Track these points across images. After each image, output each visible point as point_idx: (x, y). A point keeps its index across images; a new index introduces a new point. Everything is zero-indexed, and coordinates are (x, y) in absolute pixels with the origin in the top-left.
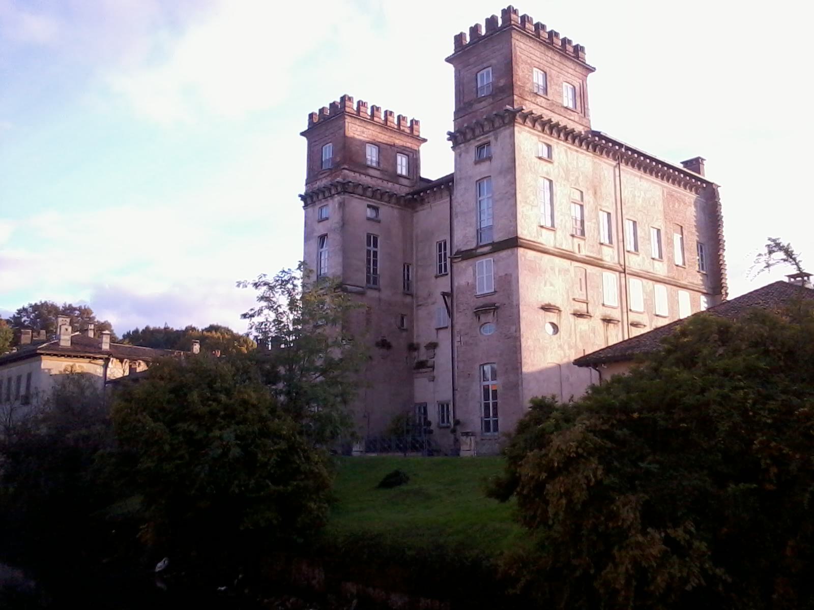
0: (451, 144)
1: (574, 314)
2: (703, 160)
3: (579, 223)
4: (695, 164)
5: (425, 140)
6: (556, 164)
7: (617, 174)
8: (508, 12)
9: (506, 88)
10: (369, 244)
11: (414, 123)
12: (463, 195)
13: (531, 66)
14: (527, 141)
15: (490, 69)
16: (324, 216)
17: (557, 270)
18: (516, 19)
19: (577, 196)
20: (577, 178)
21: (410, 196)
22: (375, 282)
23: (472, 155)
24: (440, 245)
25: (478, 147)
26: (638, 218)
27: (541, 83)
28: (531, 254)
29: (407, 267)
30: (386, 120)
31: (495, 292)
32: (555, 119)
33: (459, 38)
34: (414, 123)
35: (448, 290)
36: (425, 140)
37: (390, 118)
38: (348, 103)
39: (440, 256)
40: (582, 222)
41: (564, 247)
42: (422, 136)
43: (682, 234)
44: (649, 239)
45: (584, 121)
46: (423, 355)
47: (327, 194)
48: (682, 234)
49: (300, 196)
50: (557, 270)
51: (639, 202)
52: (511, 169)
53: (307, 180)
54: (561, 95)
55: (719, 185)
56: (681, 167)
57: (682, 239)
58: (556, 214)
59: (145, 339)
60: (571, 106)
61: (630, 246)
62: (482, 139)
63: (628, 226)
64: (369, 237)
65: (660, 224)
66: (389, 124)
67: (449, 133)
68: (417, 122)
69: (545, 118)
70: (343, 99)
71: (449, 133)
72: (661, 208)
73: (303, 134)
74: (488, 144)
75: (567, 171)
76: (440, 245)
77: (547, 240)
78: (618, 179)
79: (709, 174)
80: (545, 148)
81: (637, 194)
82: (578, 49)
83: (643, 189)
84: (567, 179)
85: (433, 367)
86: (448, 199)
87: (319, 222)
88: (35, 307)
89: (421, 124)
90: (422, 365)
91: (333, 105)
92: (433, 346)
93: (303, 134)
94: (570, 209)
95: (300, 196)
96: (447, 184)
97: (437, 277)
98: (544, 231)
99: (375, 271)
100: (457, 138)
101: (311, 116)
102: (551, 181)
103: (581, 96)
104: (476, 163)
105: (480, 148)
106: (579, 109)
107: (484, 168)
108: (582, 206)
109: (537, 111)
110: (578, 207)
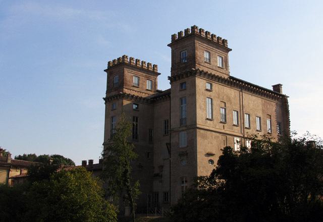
0: (169, 81)
1: (214, 155)
2: (281, 85)
3: (224, 116)
4: (277, 87)
5: (160, 74)
6: (214, 91)
7: (241, 94)
8: (194, 28)
9: (193, 59)
10: (134, 121)
11: (155, 66)
12: (175, 102)
13: (203, 54)
14: (201, 84)
15: (186, 51)
16: (114, 108)
17: (214, 137)
18: (197, 31)
19: (223, 105)
20: (223, 97)
21: (152, 99)
22: (136, 138)
23: (178, 88)
24: (166, 122)
25: (181, 84)
26: (251, 113)
27: (208, 57)
28: (202, 131)
29: (151, 131)
30: (142, 65)
31: (187, 146)
32: (213, 73)
33: (173, 36)
34: (155, 66)
35: (168, 142)
36: (160, 74)
37: (144, 65)
38: (126, 59)
39: (166, 131)
40: (225, 115)
41: (217, 127)
42: (158, 72)
43: (271, 119)
44: (256, 122)
45: (227, 72)
46: (157, 171)
47: (115, 98)
48: (271, 119)
49: (103, 98)
50: (214, 137)
51: (251, 106)
52: (194, 94)
53: (107, 91)
54: (217, 62)
55: (288, 96)
56: (272, 89)
57: (271, 121)
58: (214, 113)
59: (24, 161)
60: (221, 66)
61: (247, 125)
62: (182, 81)
63: (246, 117)
64: (134, 117)
65: (260, 114)
66: (144, 67)
67: (169, 77)
68: (156, 66)
69: (209, 73)
70: (123, 57)
71: (169, 77)
72: (261, 108)
73: (105, 71)
74: (185, 83)
75: (219, 95)
76: (166, 122)
77: (210, 125)
78: (241, 96)
79: (284, 92)
80: (209, 85)
81: (250, 102)
82: (224, 41)
83: (252, 102)
84: (219, 98)
85: (162, 176)
86: (169, 101)
87: (112, 110)
88: (55, 156)
89: (158, 67)
90: (157, 175)
91: (119, 59)
92: (162, 167)
93: (105, 71)
94: (220, 110)
95: (103, 98)
96: (168, 93)
97: (164, 136)
98: (208, 121)
99: (136, 132)
100: (172, 79)
101: (109, 63)
102: (212, 99)
103: (225, 62)
104: (180, 91)
105: (182, 84)
106: (224, 67)
107: (183, 92)
108: (225, 109)
109: (205, 70)
110: (224, 110)
